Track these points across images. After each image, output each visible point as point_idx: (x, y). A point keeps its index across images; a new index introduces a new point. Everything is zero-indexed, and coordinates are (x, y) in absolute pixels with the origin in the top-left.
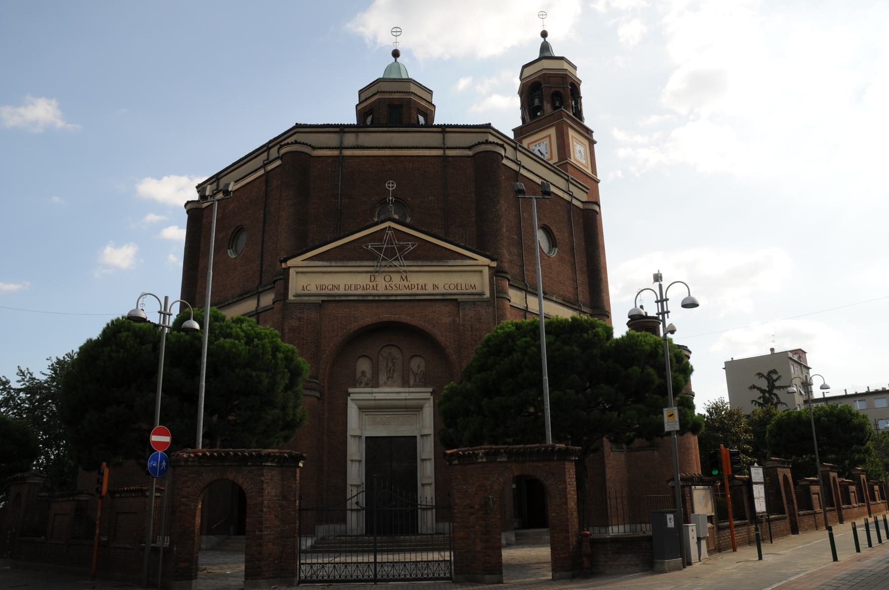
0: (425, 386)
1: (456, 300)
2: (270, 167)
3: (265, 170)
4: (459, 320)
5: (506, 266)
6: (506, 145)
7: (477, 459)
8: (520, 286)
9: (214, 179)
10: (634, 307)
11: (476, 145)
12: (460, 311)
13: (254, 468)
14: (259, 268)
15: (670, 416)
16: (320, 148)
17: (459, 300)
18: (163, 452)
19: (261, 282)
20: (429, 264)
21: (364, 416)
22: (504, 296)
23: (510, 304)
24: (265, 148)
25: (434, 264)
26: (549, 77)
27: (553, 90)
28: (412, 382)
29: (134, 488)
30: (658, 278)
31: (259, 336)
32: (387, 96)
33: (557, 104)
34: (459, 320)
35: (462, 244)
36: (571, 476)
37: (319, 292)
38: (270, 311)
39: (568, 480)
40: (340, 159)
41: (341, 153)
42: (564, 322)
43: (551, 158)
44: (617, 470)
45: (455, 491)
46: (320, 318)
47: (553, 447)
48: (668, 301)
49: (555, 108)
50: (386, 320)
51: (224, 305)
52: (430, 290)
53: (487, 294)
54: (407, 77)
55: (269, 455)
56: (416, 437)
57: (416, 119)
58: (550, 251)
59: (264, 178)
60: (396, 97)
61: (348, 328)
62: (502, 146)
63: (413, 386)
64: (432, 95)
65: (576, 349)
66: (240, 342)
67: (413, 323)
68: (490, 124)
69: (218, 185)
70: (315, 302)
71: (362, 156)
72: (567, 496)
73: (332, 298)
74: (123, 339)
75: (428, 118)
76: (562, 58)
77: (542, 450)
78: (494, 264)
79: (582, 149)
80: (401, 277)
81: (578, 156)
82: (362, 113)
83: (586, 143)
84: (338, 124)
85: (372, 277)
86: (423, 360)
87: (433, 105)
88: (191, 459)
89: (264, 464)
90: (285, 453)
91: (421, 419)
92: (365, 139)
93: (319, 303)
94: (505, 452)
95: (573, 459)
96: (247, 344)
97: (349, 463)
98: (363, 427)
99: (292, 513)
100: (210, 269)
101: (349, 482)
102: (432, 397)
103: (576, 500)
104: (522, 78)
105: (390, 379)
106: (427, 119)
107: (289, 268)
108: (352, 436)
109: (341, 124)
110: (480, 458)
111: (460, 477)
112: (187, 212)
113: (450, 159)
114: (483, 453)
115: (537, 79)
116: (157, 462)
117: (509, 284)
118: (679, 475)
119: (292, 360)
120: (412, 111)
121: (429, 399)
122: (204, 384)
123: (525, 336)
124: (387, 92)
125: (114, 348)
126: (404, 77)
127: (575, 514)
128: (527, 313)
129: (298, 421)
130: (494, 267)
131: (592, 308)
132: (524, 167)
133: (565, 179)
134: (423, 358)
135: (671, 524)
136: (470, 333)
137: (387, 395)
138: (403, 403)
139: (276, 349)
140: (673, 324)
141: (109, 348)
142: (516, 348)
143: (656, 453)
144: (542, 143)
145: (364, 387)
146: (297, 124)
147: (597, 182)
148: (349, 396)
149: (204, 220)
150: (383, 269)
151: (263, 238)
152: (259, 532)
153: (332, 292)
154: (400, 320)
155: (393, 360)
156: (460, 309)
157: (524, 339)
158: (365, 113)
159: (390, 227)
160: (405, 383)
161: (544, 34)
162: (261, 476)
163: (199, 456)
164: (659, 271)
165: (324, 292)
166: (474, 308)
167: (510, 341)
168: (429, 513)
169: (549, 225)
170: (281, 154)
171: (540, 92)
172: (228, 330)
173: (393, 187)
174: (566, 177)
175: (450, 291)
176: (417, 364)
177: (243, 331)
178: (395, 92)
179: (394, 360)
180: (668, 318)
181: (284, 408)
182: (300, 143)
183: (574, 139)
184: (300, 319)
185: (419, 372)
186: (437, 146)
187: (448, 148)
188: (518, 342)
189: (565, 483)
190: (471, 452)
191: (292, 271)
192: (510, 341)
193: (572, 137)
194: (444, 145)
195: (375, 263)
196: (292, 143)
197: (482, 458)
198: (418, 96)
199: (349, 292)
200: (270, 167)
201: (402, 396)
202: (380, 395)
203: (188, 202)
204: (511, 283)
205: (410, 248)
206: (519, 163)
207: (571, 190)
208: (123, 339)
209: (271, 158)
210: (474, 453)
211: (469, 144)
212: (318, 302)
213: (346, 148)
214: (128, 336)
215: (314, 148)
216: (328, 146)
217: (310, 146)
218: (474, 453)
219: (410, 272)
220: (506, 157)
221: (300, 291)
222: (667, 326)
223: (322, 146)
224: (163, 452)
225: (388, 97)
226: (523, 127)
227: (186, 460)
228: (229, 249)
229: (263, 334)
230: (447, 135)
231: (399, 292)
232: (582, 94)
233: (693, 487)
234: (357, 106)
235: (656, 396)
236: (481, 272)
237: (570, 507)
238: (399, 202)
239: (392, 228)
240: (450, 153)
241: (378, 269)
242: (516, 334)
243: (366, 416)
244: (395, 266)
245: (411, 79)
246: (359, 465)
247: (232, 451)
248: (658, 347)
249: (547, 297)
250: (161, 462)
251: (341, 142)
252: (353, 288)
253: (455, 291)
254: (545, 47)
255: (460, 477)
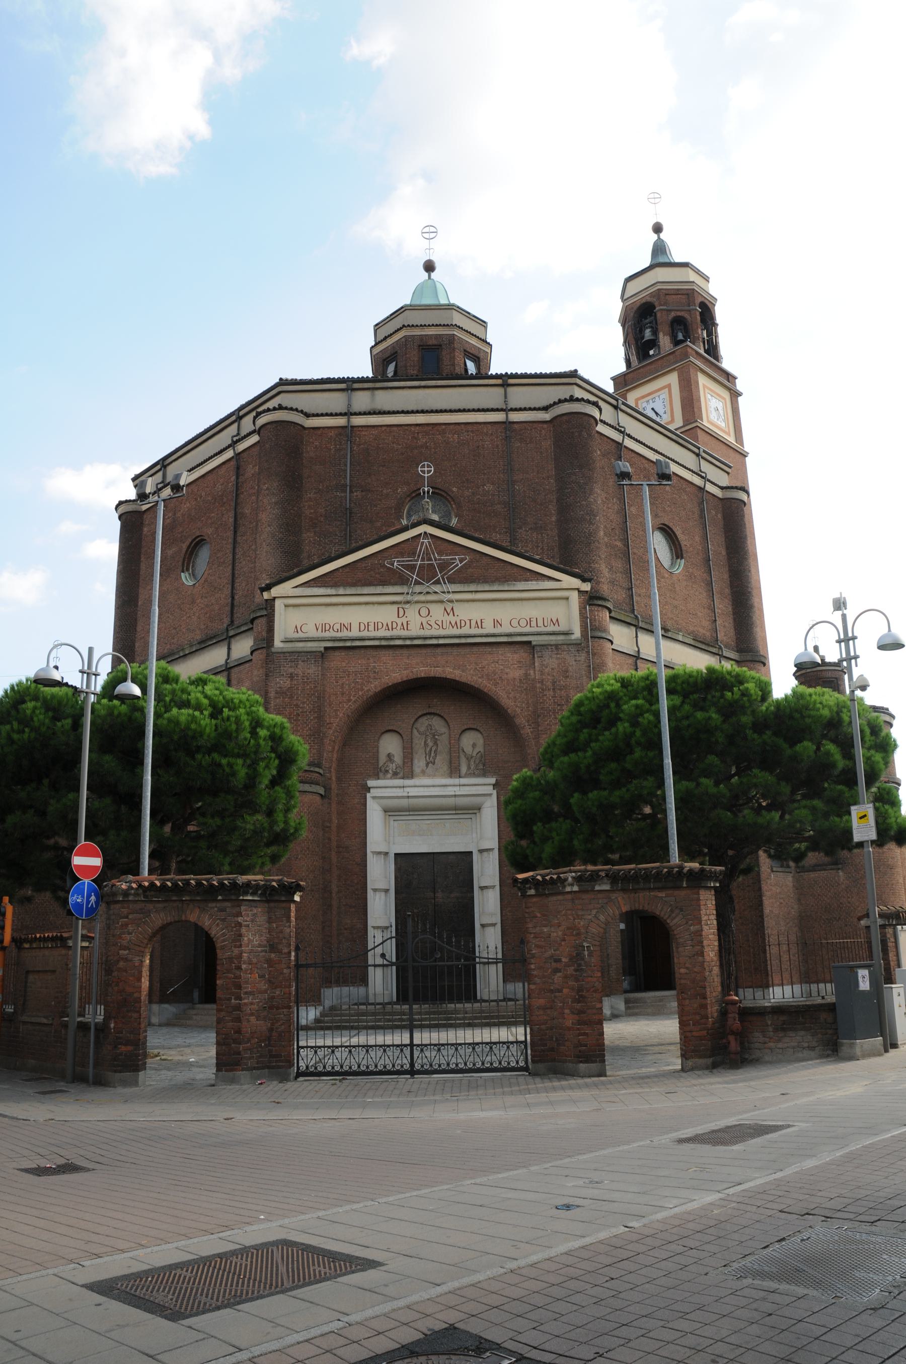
0: (484, 774)
1: (530, 642)
2: (241, 447)
3: (234, 450)
4: (535, 673)
5: (605, 589)
6: (601, 403)
7: (564, 887)
8: (628, 620)
9: (159, 467)
10: (803, 650)
11: (555, 403)
12: (536, 659)
13: (228, 904)
14: (230, 600)
15: (861, 818)
16: (317, 415)
17: (534, 643)
18: (92, 881)
19: (232, 622)
20: (487, 588)
21: (392, 822)
22: (604, 635)
23: (614, 647)
24: (234, 418)
25: (496, 587)
26: (666, 294)
27: (673, 314)
28: (464, 769)
29: (51, 935)
30: (839, 604)
31: (231, 705)
32: (418, 332)
33: (680, 336)
34: (535, 673)
35: (537, 557)
36: (708, 911)
37: (320, 634)
38: (247, 665)
39: (704, 918)
40: (348, 432)
41: (349, 421)
42: (695, 674)
43: (672, 420)
44: (782, 901)
45: (532, 936)
46: (322, 675)
47: (681, 867)
48: (856, 640)
49: (677, 343)
50: (423, 675)
51: (177, 656)
52: (489, 628)
53: (577, 634)
54: (446, 302)
55: (248, 885)
56: (471, 852)
57: (462, 365)
58: (672, 564)
59: (233, 463)
60: (431, 333)
61: (366, 689)
62: (595, 404)
63: (467, 775)
64: (486, 328)
65: (714, 715)
66: (202, 713)
67: (463, 680)
68: (576, 371)
69: (164, 476)
70: (314, 650)
71: (381, 426)
72: (702, 942)
73: (341, 644)
74: (28, 712)
75: (481, 364)
76: (686, 265)
77: (674, 872)
78: (586, 587)
79: (720, 405)
80: (445, 609)
81: (713, 416)
82: (381, 361)
83: (726, 395)
84: (344, 378)
85: (401, 610)
86: (479, 735)
87: (489, 344)
88: (133, 891)
89: (241, 898)
90: (273, 880)
91: (478, 827)
92: (385, 399)
93: (321, 652)
94: (607, 875)
95: (712, 885)
96: (212, 716)
97: (370, 894)
98: (391, 838)
99: (285, 971)
100: (155, 605)
101: (371, 922)
102: (495, 792)
103: (717, 948)
104: (625, 298)
105: (430, 765)
106: (479, 365)
107: (274, 598)
108: (374, 853)
109: (348, 378)
110: (569, 885)
111: (539, 915)
112: (120, 518)
113: (516, 426)
114: (573, 878)
115: (649, 299)
116: (83, 897)
117: (610, 617)
118: (877, 908)
119: (281, 739)
120: (457, 354)
121: (490, 795)
122: (150, 778)
123: (636, 698)
124: (417, 326)
125: (15, 725)
126: (443, 301)
127: (716, 970)
128: (638, 661)
129: (292, 831)
130: (587, 592)
131: (739, 650)
132: (629, 436)
133: (694, 452)
134: (481, 733)
135: (864, 985)
136: (551, 693)
137: (426, 789)
138: (451, 802)
139: (257, 724)
140: (865, 676)
141: (8, 727)
142: (621, 715)
143: (841, 873)
144: (657, 398)
145: (391, 778)
146: (281, 379)
147: (744, 455)
148: (369, 792)
149: (145, 529)
150: (416, 598)
151: (234, 554)
152: (235, 999)
153: (339, 635)
154: (444, 676)
155: (434, 736)
156: (536, 656)
157: (634, 702)
158: (384, 360)
159: (425, 533)
160: (454, 771)
161: (657, 229)
162: (238, 916)
163: (144, 887)
164: (841, 593)
165: (327, 635)
166: (557, 654)
167: (613, 705)
168: (493, 968)
169: (671, 525)
170: (258, 426)
171: (652, 318)
172: (184, 697)
173: (429, 472)
174: (696, 450)
175: (519, 630)
176: (472, 742)
177: (206, 697)
178: (429, 325)
179: (437, 737)
180: (856, 666)
181: (270, 813)
182: (286, 408)
183: (707, 391)
184: (291, 676)
185: (474, 754)
186: (495, 407)
187: (512, 410)
188: (625, 707)
189: (700, 923)
190: (555, 877)
191: (278, 604)
192: (613, 705)
193: (704, 386)
194: (506, 404)
195: (405, 589)
196: (275, 409)
197: (572, 885)
198: (464, 330)
199: (365, 634)
200: (241, 447)
201: (450, 791)
202: (416, 789)
203: (121, 503)
204: (613, 614)
205: (457, 565)
206: (623, 429)
207: (703, 470)
208: (28, 712)
209: (244, 432)
210: (559, 877)
211: (545, 403)
212: (318, 649)
213: (355, 414)
214: (35, 708)
215: (308, 415)
216: (329, 412)
217: (302, 412)
218: (559, 877)
219: (457, 601)
220: (601, 421)
221: (292, 635)
222: (855, 679)
223: (320, 412)
224: (92, 881)
225: (419, 334)
226: (628, 373)
227: (126, 893)
228: (183, 572)
229: (236, 701)
230: (510, 390)
231: (442, 632)
232: (718, 320)
233: (899, 927)
234: (372, 347)
235: (840, 787)
236: (567, 599)
237: (707, 958)
238: (439, 494)
239: (430, 534)
240: (515, 417)
241: (409, 598)
242: (621, 694)
243: (396, 823)
244: (436, 593)
245: (453, 305)
246: (386, 896)
247: (193, 879)
248: (842, 712)
249: (670, 636)
250: (89, 896)
251: (349, 405)
252: (371, 628)
253: (528, 629)
254: (659, 249)
255: (539, 915)
